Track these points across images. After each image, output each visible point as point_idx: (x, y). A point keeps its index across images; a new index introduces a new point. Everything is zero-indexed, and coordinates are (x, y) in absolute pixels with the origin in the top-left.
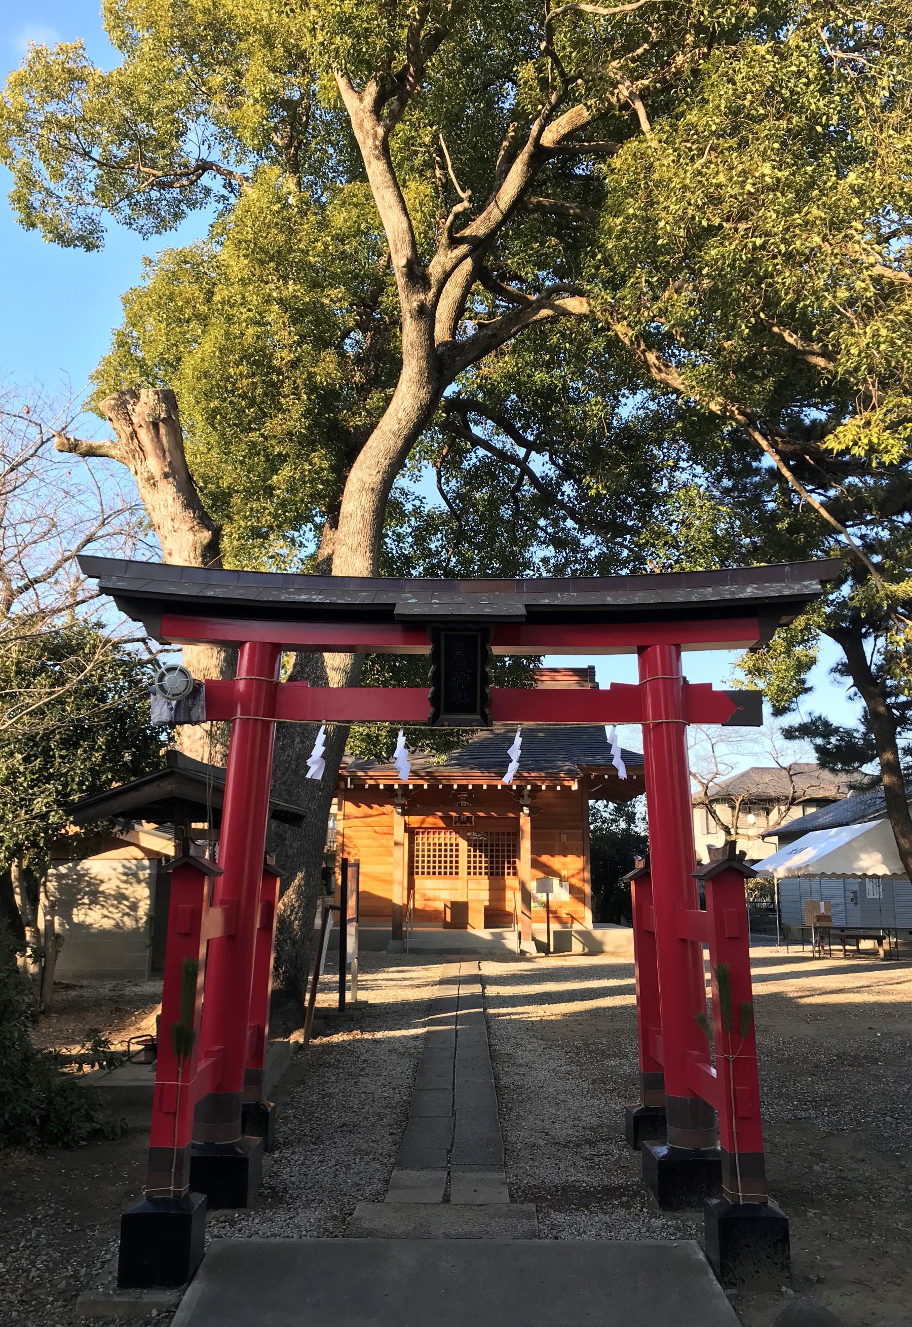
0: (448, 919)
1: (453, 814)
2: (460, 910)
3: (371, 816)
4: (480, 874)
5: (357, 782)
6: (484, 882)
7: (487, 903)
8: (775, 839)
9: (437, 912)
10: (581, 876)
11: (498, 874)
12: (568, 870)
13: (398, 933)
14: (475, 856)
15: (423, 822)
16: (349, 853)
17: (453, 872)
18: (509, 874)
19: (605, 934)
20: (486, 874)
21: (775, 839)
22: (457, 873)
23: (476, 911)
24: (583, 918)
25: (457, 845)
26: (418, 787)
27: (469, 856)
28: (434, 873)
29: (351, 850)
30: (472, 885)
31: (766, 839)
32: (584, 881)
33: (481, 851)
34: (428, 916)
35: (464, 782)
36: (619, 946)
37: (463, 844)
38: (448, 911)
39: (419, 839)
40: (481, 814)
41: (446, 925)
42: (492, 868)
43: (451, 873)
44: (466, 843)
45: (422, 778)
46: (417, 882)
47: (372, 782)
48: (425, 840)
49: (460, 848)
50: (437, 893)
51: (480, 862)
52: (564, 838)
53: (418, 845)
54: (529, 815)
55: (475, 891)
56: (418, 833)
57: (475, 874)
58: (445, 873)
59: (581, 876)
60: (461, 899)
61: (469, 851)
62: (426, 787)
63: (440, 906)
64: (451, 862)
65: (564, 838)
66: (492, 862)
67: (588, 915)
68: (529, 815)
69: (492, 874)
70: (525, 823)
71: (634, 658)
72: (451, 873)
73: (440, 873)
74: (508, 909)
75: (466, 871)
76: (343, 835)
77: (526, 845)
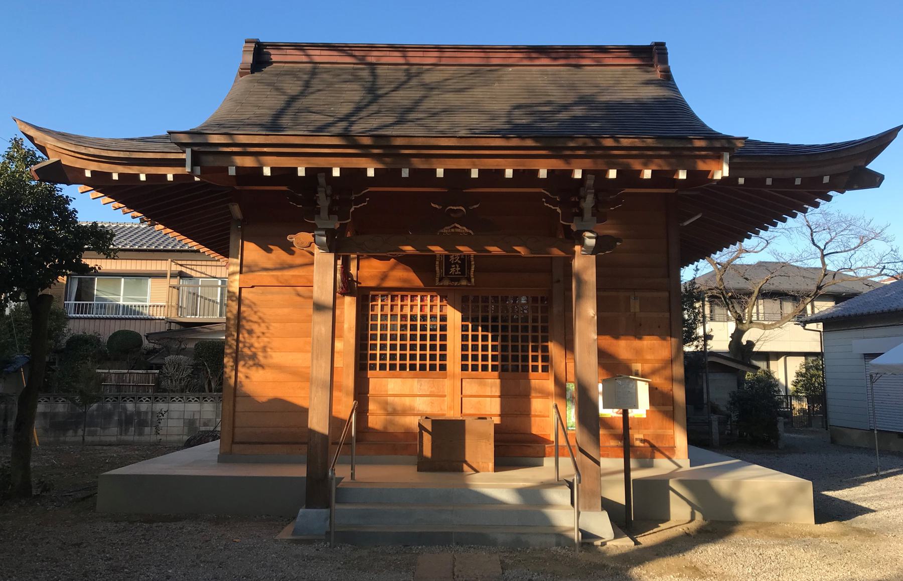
0: (427, 451)
1: (437, 249)
2: (449, 434)
3: (291, 267)
4: (485, 368)
5: (210, 161)
6: (492, 384)
7: (497, 420)
8: (820, 326)
9: (408, 433)
10: (667, 373)
11: (515, 369)
12: (644, 361)
13: (319, 490)
14: (475, 338)
15: (384, 277)
16: (250, 332)
17: (434, 365)
18: (535, 369)
19: (737, 484)
20: (494, 368)
21: (820, 326)
22: (443, 368)
23: (482, 436)
24: (672, 449)
25: (444, 318)
26: (353, 176)
27: (464, 338)
28: (393, 367)
29: (255, 327)
30: (471, 387)
31: (808, 326)
32: (672, 379)
33: (485, 329)
34: (393, 444)
35: (462, 164)
36: (767, 509)
37: (454, 317)
38: (427, 439)
39: (378, 308)
40: (495, 250)
41: (424, 465)
42: (505, 359)
43: (433, 367)
44: (458, 315)
45: (365, 152)
46: (373, 383)
47: (248, 162)
48: (387, 310)
49: (449, 323)
50: (407, 401)
51: (485, 348)
52: (635, 306)
53: (374, 317)
54: (595, 251)
55: (479, 400)
56: (374, 298)
57: (475, 368)
58: (423, 367)
59: (667, 373)
60: (453, 414)
61: (465, 328)
62: (371, 173)
63: (413, 422)
64: (433, 347)
65: (635, 306)
66: (504, 348)
67: (680, 440)
68: (595, 251)
69: (504, 369)
70: (584, 263)
71: (370, 425)
72: (433, 367)
73: (413, 367)
74: (535, 431)
75: (459, 362)
76: (240, 300)
77: (587, 312)
